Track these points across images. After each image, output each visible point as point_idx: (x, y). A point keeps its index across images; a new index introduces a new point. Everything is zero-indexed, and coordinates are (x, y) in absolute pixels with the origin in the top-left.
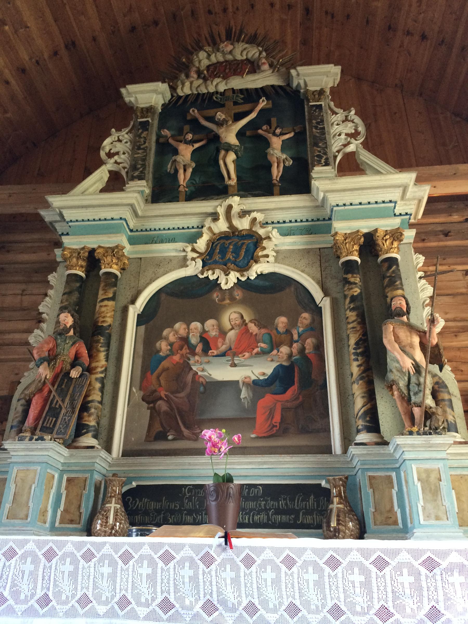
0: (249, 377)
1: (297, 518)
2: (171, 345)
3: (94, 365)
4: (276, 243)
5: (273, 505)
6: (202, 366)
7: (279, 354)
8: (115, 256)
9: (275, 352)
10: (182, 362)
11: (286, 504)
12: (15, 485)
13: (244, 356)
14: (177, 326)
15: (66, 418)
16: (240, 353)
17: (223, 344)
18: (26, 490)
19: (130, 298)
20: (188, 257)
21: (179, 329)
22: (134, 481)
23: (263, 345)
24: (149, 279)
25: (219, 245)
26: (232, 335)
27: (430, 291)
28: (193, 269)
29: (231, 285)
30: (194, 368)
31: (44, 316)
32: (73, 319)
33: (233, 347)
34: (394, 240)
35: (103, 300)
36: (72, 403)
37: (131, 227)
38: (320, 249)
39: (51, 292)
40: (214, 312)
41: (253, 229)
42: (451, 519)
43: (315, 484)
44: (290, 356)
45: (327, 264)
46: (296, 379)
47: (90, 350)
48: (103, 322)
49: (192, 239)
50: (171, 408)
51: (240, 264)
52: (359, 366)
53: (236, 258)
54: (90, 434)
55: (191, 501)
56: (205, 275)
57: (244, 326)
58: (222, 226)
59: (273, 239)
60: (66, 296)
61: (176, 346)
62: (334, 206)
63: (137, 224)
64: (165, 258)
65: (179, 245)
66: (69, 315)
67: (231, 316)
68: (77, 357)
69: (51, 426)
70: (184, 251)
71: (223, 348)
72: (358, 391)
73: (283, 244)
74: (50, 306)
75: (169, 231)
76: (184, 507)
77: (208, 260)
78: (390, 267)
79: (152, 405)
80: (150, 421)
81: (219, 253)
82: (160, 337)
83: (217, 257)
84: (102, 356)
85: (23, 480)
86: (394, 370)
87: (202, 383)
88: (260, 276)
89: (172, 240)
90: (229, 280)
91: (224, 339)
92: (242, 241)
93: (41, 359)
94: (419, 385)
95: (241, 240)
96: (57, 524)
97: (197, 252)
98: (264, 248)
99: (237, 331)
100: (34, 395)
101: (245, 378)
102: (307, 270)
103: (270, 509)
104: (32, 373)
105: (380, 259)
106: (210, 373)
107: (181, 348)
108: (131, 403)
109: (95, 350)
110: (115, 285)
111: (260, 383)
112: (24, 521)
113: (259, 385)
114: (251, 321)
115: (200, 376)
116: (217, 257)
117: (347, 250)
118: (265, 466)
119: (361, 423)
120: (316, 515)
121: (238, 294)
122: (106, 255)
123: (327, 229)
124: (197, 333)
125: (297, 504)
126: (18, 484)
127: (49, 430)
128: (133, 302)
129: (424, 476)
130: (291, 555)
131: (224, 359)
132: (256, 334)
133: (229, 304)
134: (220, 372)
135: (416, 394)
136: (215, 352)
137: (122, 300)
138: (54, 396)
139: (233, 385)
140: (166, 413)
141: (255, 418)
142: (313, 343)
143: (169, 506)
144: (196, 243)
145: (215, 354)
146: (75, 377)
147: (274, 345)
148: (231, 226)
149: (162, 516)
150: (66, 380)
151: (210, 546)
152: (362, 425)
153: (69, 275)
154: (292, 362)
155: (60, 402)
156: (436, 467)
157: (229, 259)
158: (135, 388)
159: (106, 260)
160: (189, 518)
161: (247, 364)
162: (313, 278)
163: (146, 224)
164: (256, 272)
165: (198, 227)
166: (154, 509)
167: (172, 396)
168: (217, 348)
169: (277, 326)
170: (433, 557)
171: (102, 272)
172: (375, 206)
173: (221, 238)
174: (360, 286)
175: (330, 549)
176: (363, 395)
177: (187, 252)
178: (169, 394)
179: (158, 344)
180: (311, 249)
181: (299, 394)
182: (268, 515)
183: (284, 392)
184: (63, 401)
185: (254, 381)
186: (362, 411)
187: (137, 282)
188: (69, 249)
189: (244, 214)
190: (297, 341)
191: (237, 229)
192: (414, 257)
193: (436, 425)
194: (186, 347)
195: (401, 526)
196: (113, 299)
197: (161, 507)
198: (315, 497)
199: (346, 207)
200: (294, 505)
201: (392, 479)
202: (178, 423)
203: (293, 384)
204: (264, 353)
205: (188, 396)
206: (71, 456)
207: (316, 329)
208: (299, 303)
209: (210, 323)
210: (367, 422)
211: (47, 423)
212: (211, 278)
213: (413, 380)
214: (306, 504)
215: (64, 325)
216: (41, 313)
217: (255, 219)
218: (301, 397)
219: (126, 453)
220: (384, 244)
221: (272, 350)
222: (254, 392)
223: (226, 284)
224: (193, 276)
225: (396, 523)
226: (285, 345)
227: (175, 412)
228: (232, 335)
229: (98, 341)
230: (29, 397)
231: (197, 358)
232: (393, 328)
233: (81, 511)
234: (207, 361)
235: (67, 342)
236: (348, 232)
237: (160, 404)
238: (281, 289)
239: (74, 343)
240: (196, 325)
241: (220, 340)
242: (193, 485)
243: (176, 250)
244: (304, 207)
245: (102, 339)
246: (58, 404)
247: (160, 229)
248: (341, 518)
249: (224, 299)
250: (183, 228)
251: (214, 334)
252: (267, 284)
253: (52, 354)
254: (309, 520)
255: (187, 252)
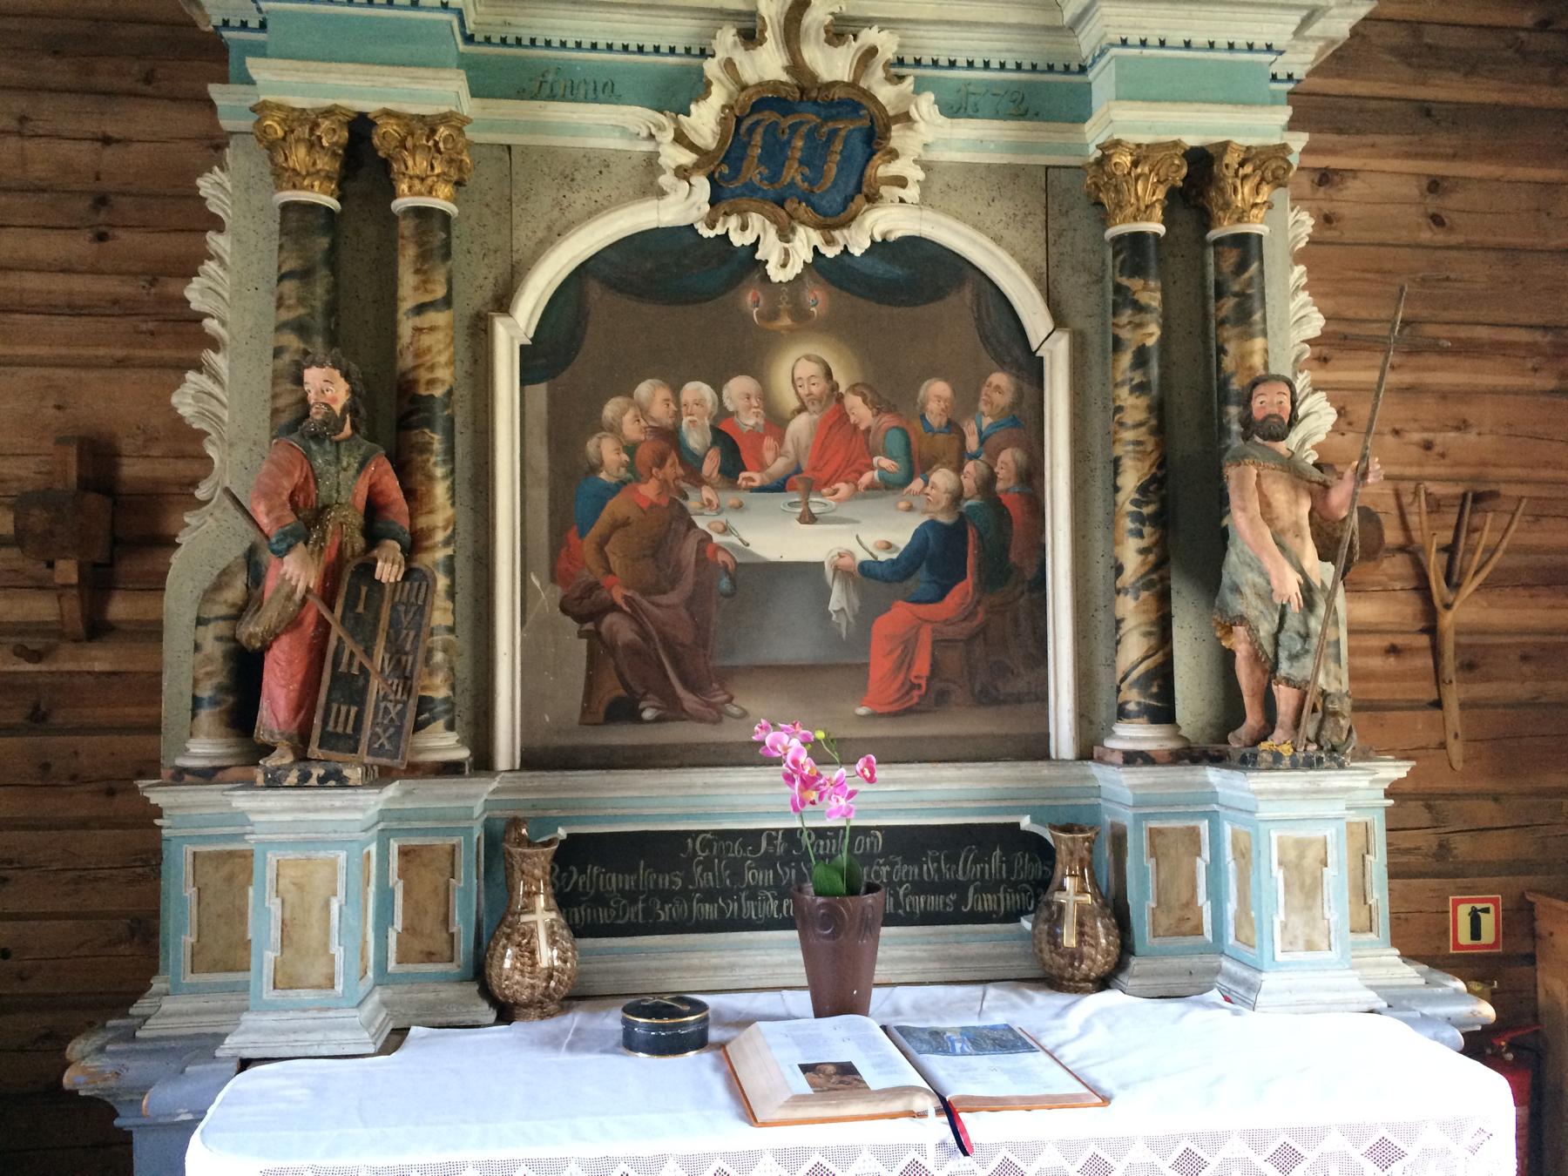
0: (851, 554)
1: (963, 899)
2: (631, 449)
3: (423, 522)
4: (929, 140)
5: (907, 874)
6: (722, 518)
7: (928, 490)
8: (438, 151)
9: (917, 484)
10: (664, 502)
11: (939, 870)
12: (278, 901)
13: (836, 492)
14: (644, 389)
15: (391, 706)
16: (826, 485)
17: (777, 455)
18: (316, 914)
19: (488, 293)
20: (662, 160)
21: (651, 400)
22: (561, 825)
23: (885, 462)
24: (543, 225)
25: (760, 130)
26: (800, 426)
27: (1315, 324)
28: (683, 205)
29: (795, 268)
30: (701, 523)
31: (211, 325)
32: (347, 386)
33: (805, 465)
34: (1263, 179)
35: (420, 309)
36: (399, 661)
37: (471, 27)
38: (1047, 168)
39: (216, 242)
40: (745, 354)
41: (863, 84)
42: (1337, 948)
43: (1005, 825)
44: (957, 497)
45: (1064, 222)
46: (971, 561)
47: (402, 468)
48: (431, 383)
49: (676, 92)
50: (645, 636)
51: (824, 203)
52: (1143, 551)
53: (811, 183)
54: (441, 723)
55: (712, 870)
56: (719, 230)
57: (834, 403)
58: (768, 64)
59: (921, 126)
60: (290, 286)
61: (645, 454)
62: (1112, 45)
63: (489, 19)
64: (588, 154)
65: (637, 116)
66: (337, 373)
67: (797, 368)
68: (374, 508)
69: (349, 730)
70: (651, 137)
71: (779, 466)
72: (1132, 611)
73: (947, 144)
74: (226, 295)
75: (594, 56)
76: (693, 883)
77: (727, 174)
78: (1242, 266)
79: (589, 626)
80: (588, 670)
81: (761, 160)
82: (594, 425)
83: (754, 173)
84: (441, 490)
85: (299, 886)
86: (1246, 590)
87: (726, 566)
88: (880, 248)
89: (603, 90)
90: (786, 253)
91: (780, 439)
92: (831, 125)
93: (284, 535)
94: (1305, 637)
95: (826, 120)
96: (392, 965)
97: (692, 147)
98: (894, 155)
99: (816, 417)
100: (277, 637)
101: (841, 556)
102: (1009, 235)
103: (901, 884)
104: (210, 520)
105: (1214, 234)
106: (746, 539)
107: (661, 462)
108: (530, 618)
109: (419, 477)
110: (447, 255)
111: (878, 570)
112: (324, 992)
113: (875, 577)
114: (853, 388)
115: (718, 548)
116: (754, 173)
117: (1138, 199)
118: (892, 788)
119: (1133, 698)
120: (1005, 891)
121: (817, 299)
122: (409, 143)
123: (1077, 108)
124: (702, 417)
125: (963, 870)
126: (288, 897)
127: (348, 742)
128: (504, 302)
129: (1292, 855)
130: (1102, 1154)
131: (780, 500)
132: (868, 430)
133: (791, 330)
134: (773, 536)
135: (1294, 657)
136: (758, 479)
137: (472, 297)
138: (340, 638)
139: (809, 572)
140: (630, 648)
141: (866, 665)
142: (1015, 461)
143: (656, 883)
144: (688, 114)
145: (757, 484)
146: (392, 580)
147: (917, 465)
148: (796, 66)
149: (640, 905)
150: (364, 589)
151: (920, 1148)
152: (1139, 704)
153: (286, 207)
154: (961, 515)
155: (360, 657)
156: (1320, 834)
157: (792, 184)
158: (538, 577)
159: (410, 163)
160: (709, 911)
161: (845, 515)
162: (1025, 264)
163: (522, 20)
164: (872, 237)
165: (688, 51)
166: (618, 891)
167: (645, 603)
168: (762, 467)
169: (923, 407)
170: (1390, 1138)
171: (399, 204)
172: (1226, 56)
173: (760, 105)
174: (1138, 443)
175: (1182, 1136)
176: (1148, 629)
177: (658, 144)
178: (637, 597)
179: (591, 446)
180: (1023, 167)
181: (978, 602)
182: (896, 895)
183: (941, 597)
184: (369, 652)
185: (862, 565)
186: (1142, 668)
187: (507, 232)
188: (279, 107)
189: (839, 31)
190: (974, 457)
191: (814, 77)
192: (1291, 217)
193: (1335, 740)
194: (672, 458)
195: (1208, 936)
196: (447, 302)
197: (637, 885)
198: (1005, 853)
199: (1146, 52)
200: (956, 872)
201: (1198, 835)
202: (667, 677)
203: (962, 576)
204: (888, 486)
205: (690, 602)
206: (407, 793)
207: (1026, 423)
208: (985, 339)
209: (739, 388)
210: (1152, 696)
211: (336, 722)
212: (738, 239)
213: (1293, 622)
214: (983, 870)
215: (324, 409)
216: (199, 317)
217: (872, 52)
218: (980, 609)
219: (534, 759)
220: (1235, 191)
221: (910, 478)
222: (863, 597)
223: (784, 266)
224: (679, 228)
225: (1198, 930)
226: (944, 465)
227: (659, 644)
228: (800, 426)
229: (425, 448)
230: (263, 642)
231: (706, 493)
232: (1258, 475)
233: (454, 929)
234: (736, 502)
235: (345, 464)
236: (1146, 139)
237: (612, 624)
238: (938, 294)
239: (363, 465)
240: (697, 391)
241: (769, 442)
242: (715, 832)
243: (624, 132)
244: (1021, 27)
245: (437, 441)
246: (356, 664)
247: (563, 44)
248: (1087, 929)
249: (773, 315)
250: (641, 50)
251: (751, 422)
252: (898, 271)
253: (305, 504)
254: (988, 903)
255: (658, 144)
